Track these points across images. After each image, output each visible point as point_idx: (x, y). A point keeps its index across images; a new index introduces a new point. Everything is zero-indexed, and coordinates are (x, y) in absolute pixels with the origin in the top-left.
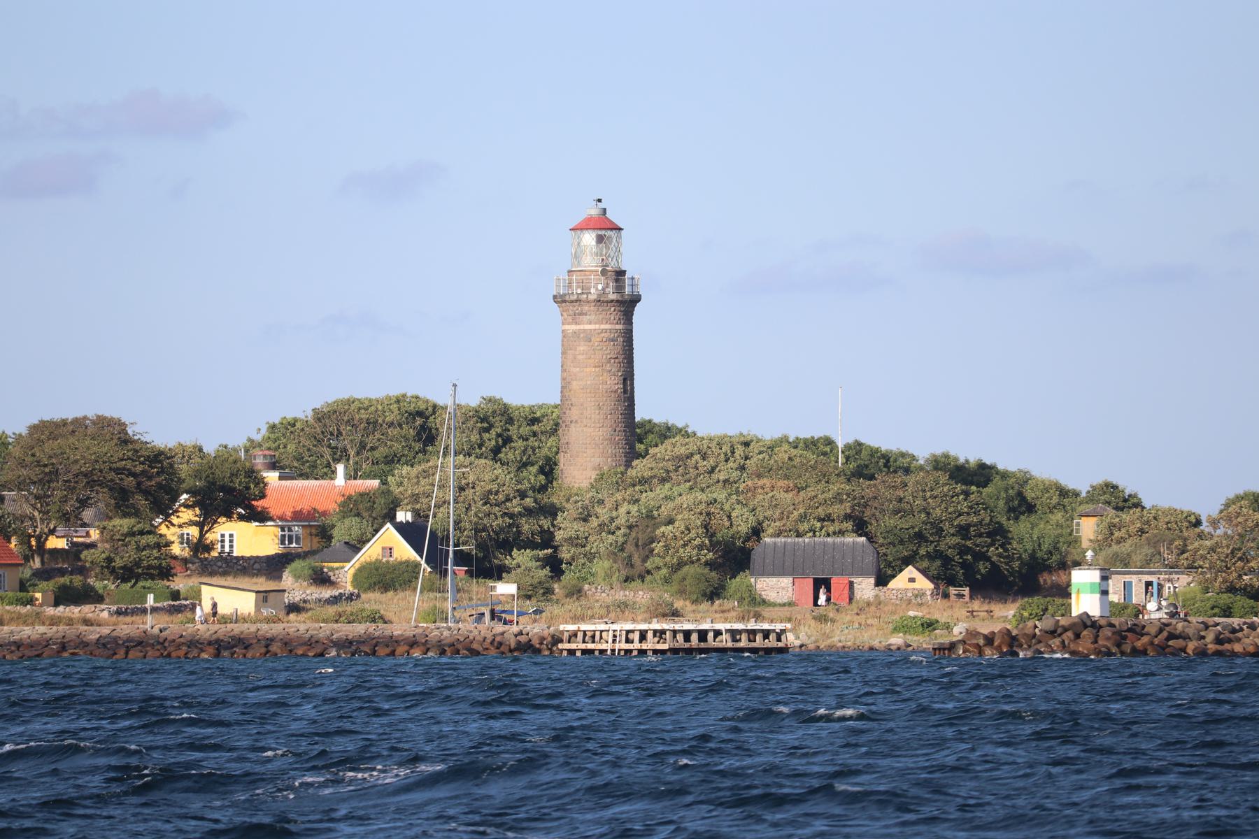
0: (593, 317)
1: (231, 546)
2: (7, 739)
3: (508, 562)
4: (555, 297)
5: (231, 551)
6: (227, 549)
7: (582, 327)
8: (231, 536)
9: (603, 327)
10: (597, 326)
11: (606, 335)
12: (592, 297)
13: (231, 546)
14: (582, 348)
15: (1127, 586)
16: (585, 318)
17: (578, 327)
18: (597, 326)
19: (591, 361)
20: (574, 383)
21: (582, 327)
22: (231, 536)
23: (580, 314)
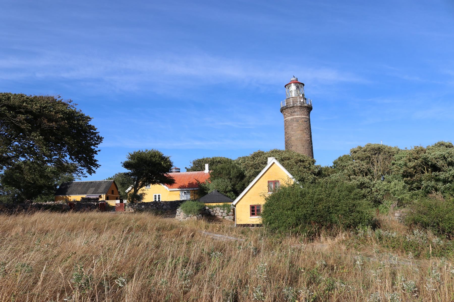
0: (299, 113)
1: (159, 198)
2: (453, 185)
3: (96, 149)
4: (252, 208)
5: (159, 200)
6: (157, 200)
7: (294, 117)
8: (159, 196)
9: (303, 116)
10: (300, 116)
11: (304, 119)
12: (299, 104)
13: (159, 198)
14: (295, 124)
15: (443, 263)
16: (296, 113)
17: (293, 117)
18: (300, 116)
19: (299, 129)
20: (293, 138)
21: (294, 117)
22: (159, 196)
23: (293, 112)
